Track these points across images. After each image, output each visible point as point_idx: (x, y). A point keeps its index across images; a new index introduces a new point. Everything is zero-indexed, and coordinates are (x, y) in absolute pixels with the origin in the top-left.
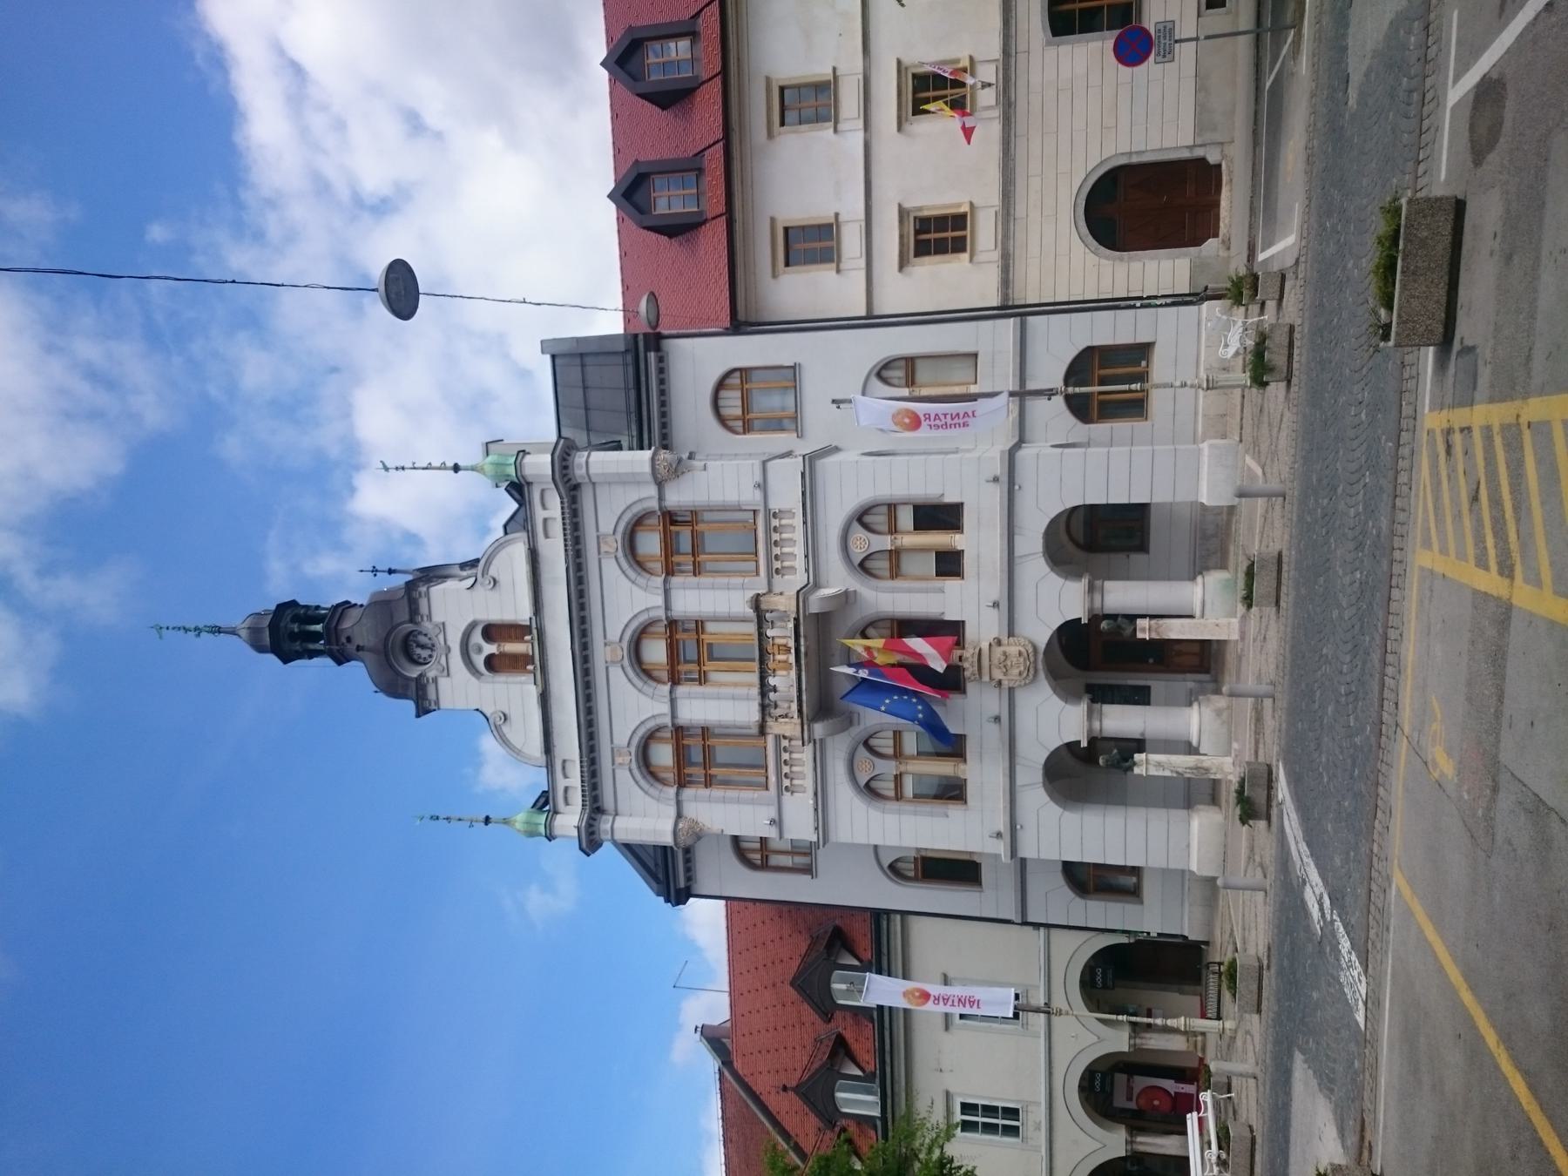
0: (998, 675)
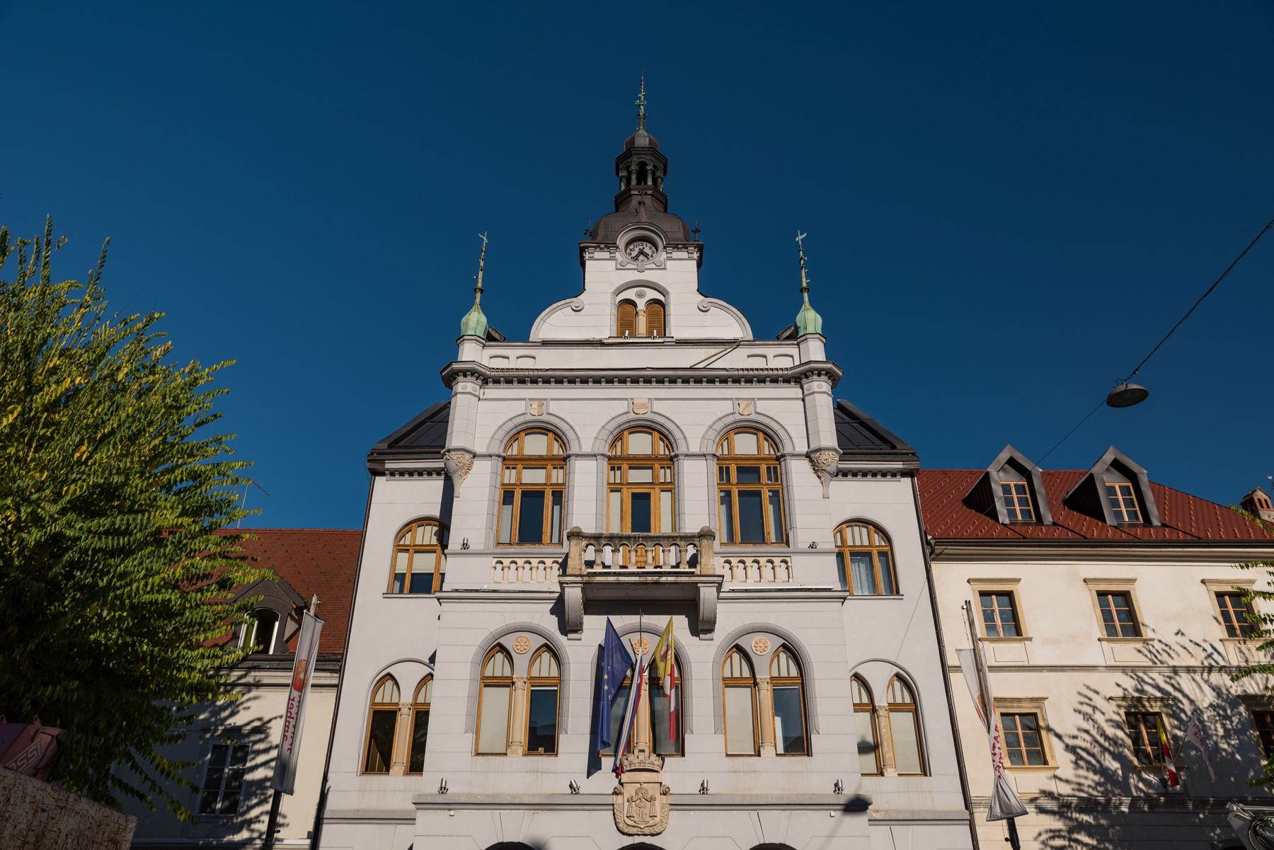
0: (629, 791)
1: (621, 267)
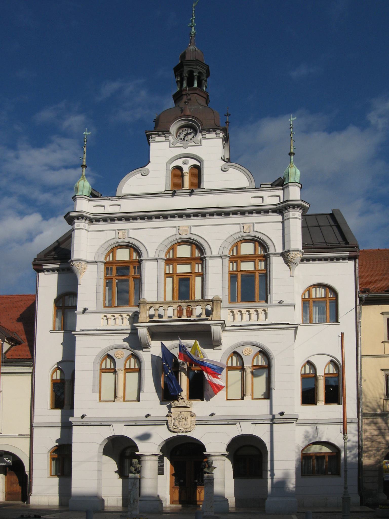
0: (174, 415)
1: (172, 146)
